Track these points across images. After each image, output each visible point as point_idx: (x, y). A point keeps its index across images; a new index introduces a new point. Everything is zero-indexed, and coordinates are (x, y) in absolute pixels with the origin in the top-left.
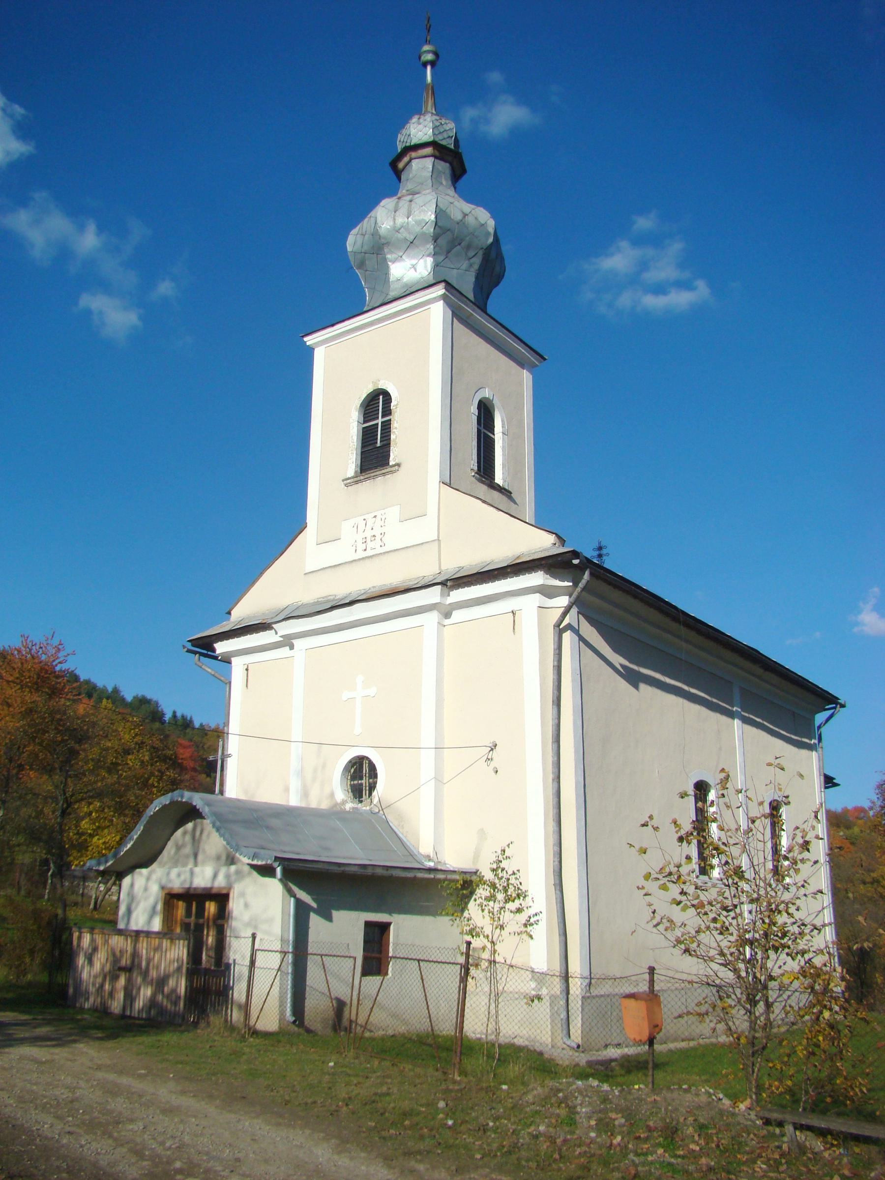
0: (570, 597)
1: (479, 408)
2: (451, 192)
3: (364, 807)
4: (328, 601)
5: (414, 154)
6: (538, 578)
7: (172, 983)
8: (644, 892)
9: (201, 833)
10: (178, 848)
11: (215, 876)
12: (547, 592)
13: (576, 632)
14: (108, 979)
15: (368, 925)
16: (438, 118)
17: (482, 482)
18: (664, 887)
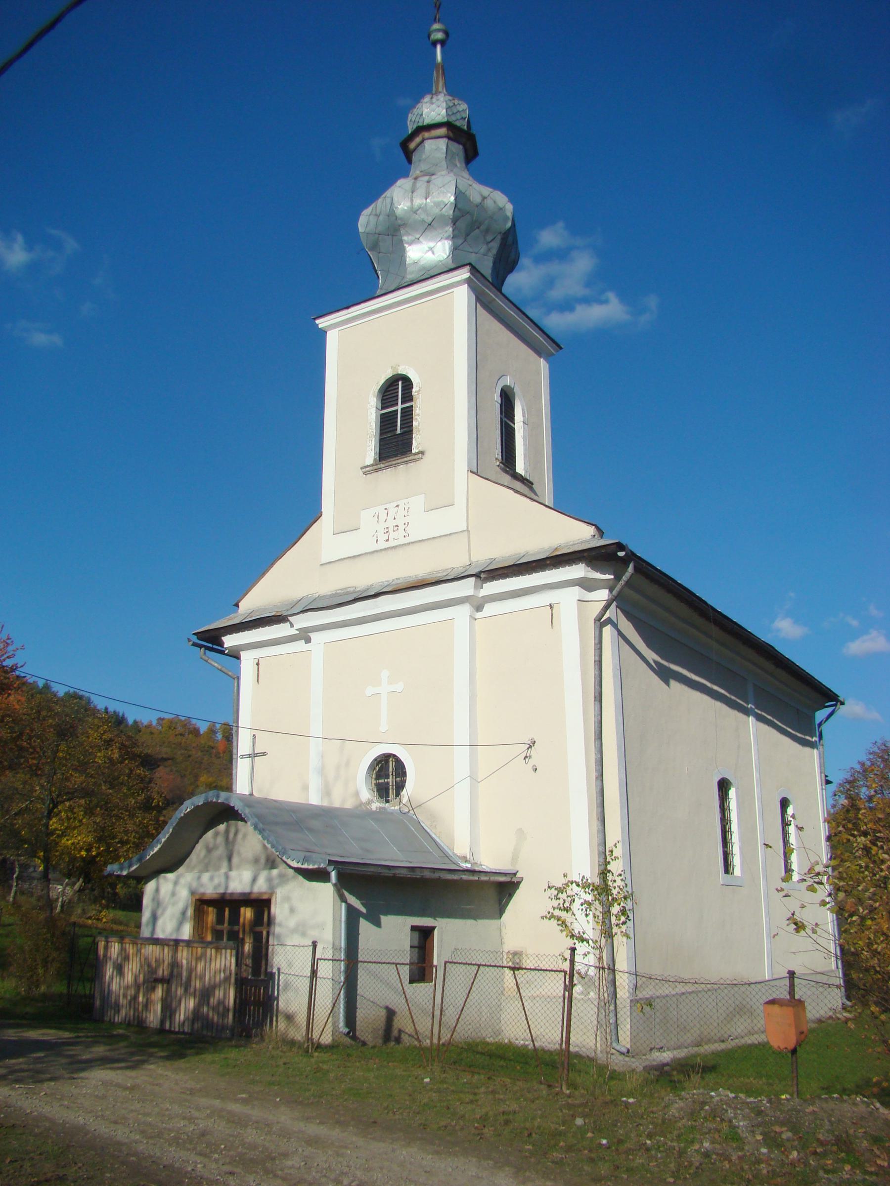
0: (611, 591)
1: (501, 396)
2: (466, 174)
3: (393, 807)
4: (347, 593)
5: (426, 135)
6: (579, 571)
7: (219, 994)
8: (783, 893)
9: (236, 834)
10: (209, 850)
11: (254, 880)
12: (587, 585)
13: (615, 626)
14: (141, 990)
15: (414, 928)
16: (450, 98)
17: (507, 472)
18: (811, 889)
